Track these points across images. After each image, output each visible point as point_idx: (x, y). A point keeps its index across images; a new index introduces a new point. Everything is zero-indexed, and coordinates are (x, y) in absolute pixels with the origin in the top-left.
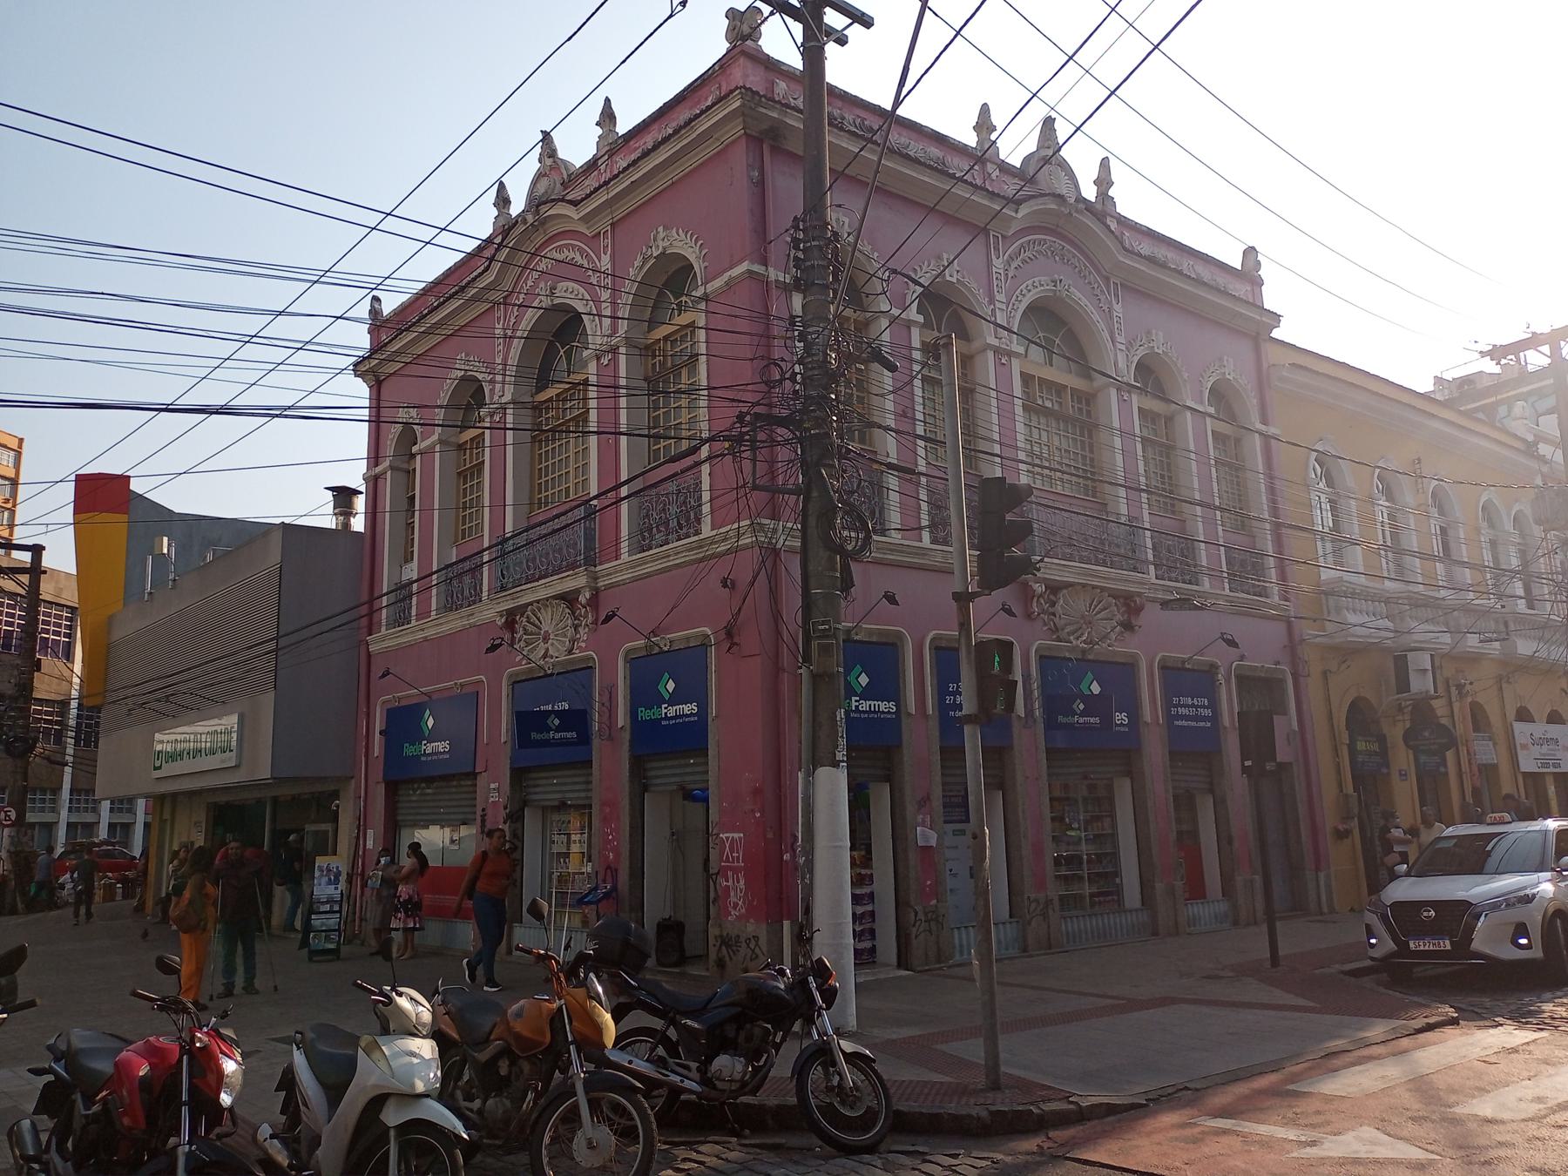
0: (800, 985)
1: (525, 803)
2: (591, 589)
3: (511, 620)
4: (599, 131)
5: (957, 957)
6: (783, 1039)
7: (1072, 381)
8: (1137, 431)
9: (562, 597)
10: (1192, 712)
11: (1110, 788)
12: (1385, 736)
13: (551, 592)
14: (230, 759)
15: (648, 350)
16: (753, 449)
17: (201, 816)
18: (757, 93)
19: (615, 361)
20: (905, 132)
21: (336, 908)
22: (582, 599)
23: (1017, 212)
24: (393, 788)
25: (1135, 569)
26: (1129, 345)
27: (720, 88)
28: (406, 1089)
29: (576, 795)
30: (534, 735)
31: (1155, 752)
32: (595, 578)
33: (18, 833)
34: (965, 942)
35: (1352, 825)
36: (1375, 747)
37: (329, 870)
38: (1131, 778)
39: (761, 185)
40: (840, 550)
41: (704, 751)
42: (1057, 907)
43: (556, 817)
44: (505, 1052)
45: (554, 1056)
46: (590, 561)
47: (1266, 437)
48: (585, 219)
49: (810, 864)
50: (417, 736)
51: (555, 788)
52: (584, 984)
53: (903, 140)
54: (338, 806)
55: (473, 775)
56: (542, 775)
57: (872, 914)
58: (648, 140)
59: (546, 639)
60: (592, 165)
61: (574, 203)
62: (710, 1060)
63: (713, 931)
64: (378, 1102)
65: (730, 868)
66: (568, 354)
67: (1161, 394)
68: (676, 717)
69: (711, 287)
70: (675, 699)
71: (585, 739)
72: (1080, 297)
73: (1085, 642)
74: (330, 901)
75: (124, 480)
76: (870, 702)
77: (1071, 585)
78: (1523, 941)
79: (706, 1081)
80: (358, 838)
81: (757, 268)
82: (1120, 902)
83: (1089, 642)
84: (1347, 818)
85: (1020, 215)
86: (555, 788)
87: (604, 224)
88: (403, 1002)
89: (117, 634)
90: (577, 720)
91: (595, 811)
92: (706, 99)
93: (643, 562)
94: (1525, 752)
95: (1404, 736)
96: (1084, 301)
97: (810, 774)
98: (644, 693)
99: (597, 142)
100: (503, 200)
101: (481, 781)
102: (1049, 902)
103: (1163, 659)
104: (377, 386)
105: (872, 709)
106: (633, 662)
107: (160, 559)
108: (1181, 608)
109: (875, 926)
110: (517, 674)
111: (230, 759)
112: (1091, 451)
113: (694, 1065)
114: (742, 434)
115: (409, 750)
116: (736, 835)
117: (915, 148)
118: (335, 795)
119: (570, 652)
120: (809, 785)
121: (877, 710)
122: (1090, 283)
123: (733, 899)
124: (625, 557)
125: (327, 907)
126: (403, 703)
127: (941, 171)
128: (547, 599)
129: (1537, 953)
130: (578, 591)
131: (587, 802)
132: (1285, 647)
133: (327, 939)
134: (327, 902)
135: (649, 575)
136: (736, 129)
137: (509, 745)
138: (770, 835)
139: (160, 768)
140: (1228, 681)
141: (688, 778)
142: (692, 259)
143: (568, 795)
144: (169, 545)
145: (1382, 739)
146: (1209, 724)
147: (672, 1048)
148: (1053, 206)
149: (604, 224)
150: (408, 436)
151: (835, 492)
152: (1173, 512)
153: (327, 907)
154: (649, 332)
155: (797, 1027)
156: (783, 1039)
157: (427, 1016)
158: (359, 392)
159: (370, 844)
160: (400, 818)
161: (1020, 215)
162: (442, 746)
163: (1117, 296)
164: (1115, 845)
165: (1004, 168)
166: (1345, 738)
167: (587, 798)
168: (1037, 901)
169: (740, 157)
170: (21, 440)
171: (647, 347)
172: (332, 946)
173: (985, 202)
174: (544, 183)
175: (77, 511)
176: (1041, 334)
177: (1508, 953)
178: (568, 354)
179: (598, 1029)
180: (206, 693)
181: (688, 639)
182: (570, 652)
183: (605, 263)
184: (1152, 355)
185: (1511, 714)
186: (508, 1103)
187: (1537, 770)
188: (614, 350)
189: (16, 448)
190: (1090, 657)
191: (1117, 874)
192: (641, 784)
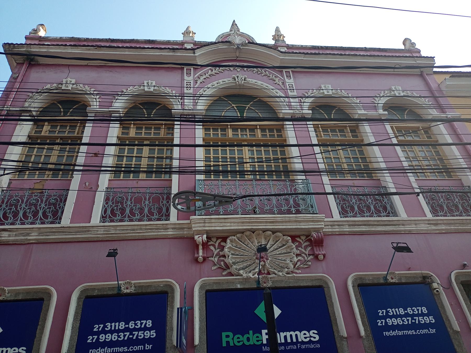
10: (407, 321)
76: (285, 334)
77: (234, 233)
96: (265, 85)
99: (17, 44)
105: (289, 340)
121: (294, 340)
146: (433, 331)
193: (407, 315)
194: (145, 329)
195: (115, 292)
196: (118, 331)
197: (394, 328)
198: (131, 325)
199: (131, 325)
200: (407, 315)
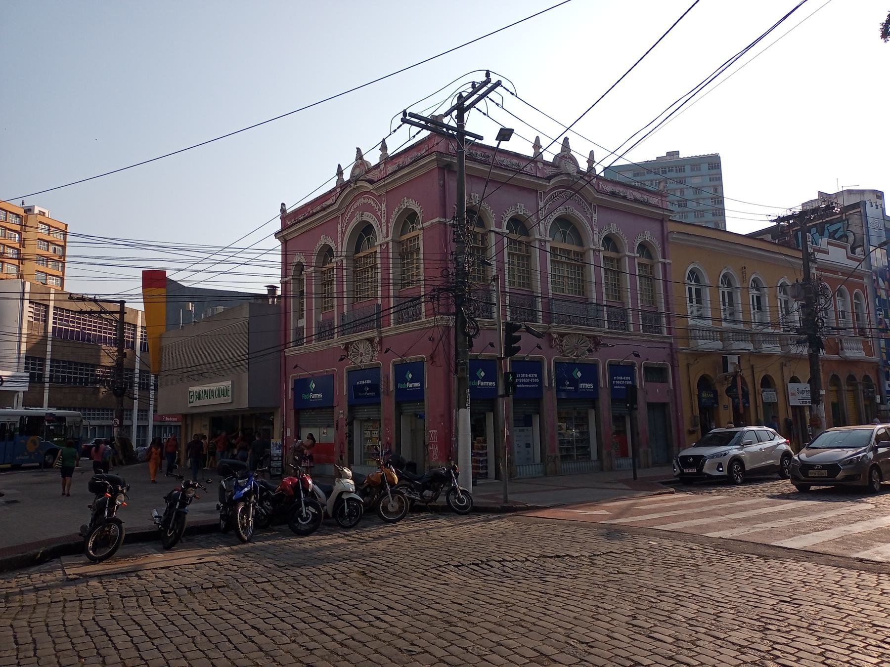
0: (449, 472)
1: (354, 418)
2: (379, 337)
3: (347, 346)
4: (380, 153)
5: (518, 476)
6: (443, 486)
7: (574, 248)
8: (602, 265)
9: (368, 339)
10: (528, 380)
11: (587, 413)
12: (717, 391)
13: (363, 337)
14: (228, 399)
15: (401, 243)
16: (438, 301)
17: (207, 422)
18: (442, 153)
19: (387, 247)
20: (502, 155)
21: (280, 459)
22: (375, 341)
23: (549, 183)
24: (298, 412)
25: (598, 326)
26: (600, 231)
27: (428, 146)
28: (348, 490)
29: (374, 416)
30: (360, 394)
31: (604, 399)
32: (381, 333)
33: (121, 429)
34: (522, 471)
35: (697, 428)
36: (712, 396)
37: (276, 444)
38: (595, 410)
39: (444, 186)
40: (467, 334)
41: (423, 401)
42: (560, 459)
43: (366, 424)
44: (369, 486)
45: (382, 486)
46: (379, 327)
47: (664, 264)
48: (375, 189)
49: (457, 440)
50: (308, 391)
51: (366, 413)
52: (389, 468)
53: (502, 159)
54: (273, 419)
55: (333, 407)
56: (361, 408)
57: (486, 460)
58: (400, 161)
59: (361, 355)
60: (377, 166)
61: (371, 182)
62: (423, 492)
63: (427, 465)
64: (341, 493)
65: (433, 443)
66: (368, 239)
67: (616, 249)
68: (412, 388)
69: (426, 224)
70: (412, 381)
71: (378, 395)
72: (578, 214)
73: (575, 356)
74: (278, 456)
75: (163, 273)
78: (721, 469)
79: (422, 497)
80: (283, 432)
81: (443, 220)
82: (590, 458)
83: (577, 356)
84: (695, 425)
85: (550, 184)
86: (366, 413)
87: (383, 192)
88: (345, 470)
89: (165, 342)
90: (375, 387)
91: (382, 422)
92: (423, 150)
93: (399, 328)
94: (794, 397)
95: (838, 377)
97: (457, 411)
98: (400, 377)
100: (340, 172)
101: (336, 409)
102: (556, 457)
103: (610, 362)
104: (285, 242)
106: (396, 366)
107: (187, 313)
108: (604, 347)
109: (488, 465)
110: (350, 368)
111: (228, 400)
112: (582, 276)
113: (419, 493)
114: (434, 295)
115: (304, 397)
116: (435, 431)
117: (506, 161)
118: (272, 414)
119: (371, 361)
120: (457, 415)
122: (582, 207)
123: (434, 454)
124: (392, 326)
125: (277, 458)
126: (301, 377)
127: (519, 171)
128: (362, 340)
129: (725, 473)
130: (374, 338)
131: (378, 418)
132: (669, 354)
133: (277, 471)
134: (276, 457)
135: (401, 333)
136: (435, 165)
137: (347, 396)
138: (447, 431)
139: (193, 402)
140: (640, 369)
141: (417, 410)
142: (416, 210)
143: (371, 416)
144: (192, 306)
145: (715, 393)
147: (412, 489)
148: (566, 178)
149: (383, 192)
150: (300, 267)
151: (466, 315)
152: (619, 299)
153: (277, 458)
154: (401, 236)
155: (447, 484)
156: (443, 486)
157: (351, 475)
158: (278, 243)
159: (288, 434)
160: (301, 424)
161: (550, 184)
162: (319, 395)
163: (595, 210)
164: (588, 435)
165: (546, 163)
166: (696, 392)
167: (378, 417)
168: (551, 456)
169: (436, 174)
170: (66, 225)
171: (400, 242)
172: (279, 473)
173: (536, 181)
174: (357, 171)
175: (144, 287)
176: (561, 230)
177: (716, 473)
178: (368, 239)
179: (393, 479)
180: (217, 373)
181: (417, 358)
182: (371, 361)
183: (383, 207)
184: (611, 234)
185: (787, 379)
186: (370, 498)
187: (800, 405)
188: (387, 243)
189: (64, 229)
190: (577, 362)
191: (589, 447)
192: (399, 412)
193: (623, 380)
194: (535, 378)
195: (522, 359)
196: (526, 378)
197: (522, 383)
198: (530, 375)
199: (530, 375)
200: (528, 378)
